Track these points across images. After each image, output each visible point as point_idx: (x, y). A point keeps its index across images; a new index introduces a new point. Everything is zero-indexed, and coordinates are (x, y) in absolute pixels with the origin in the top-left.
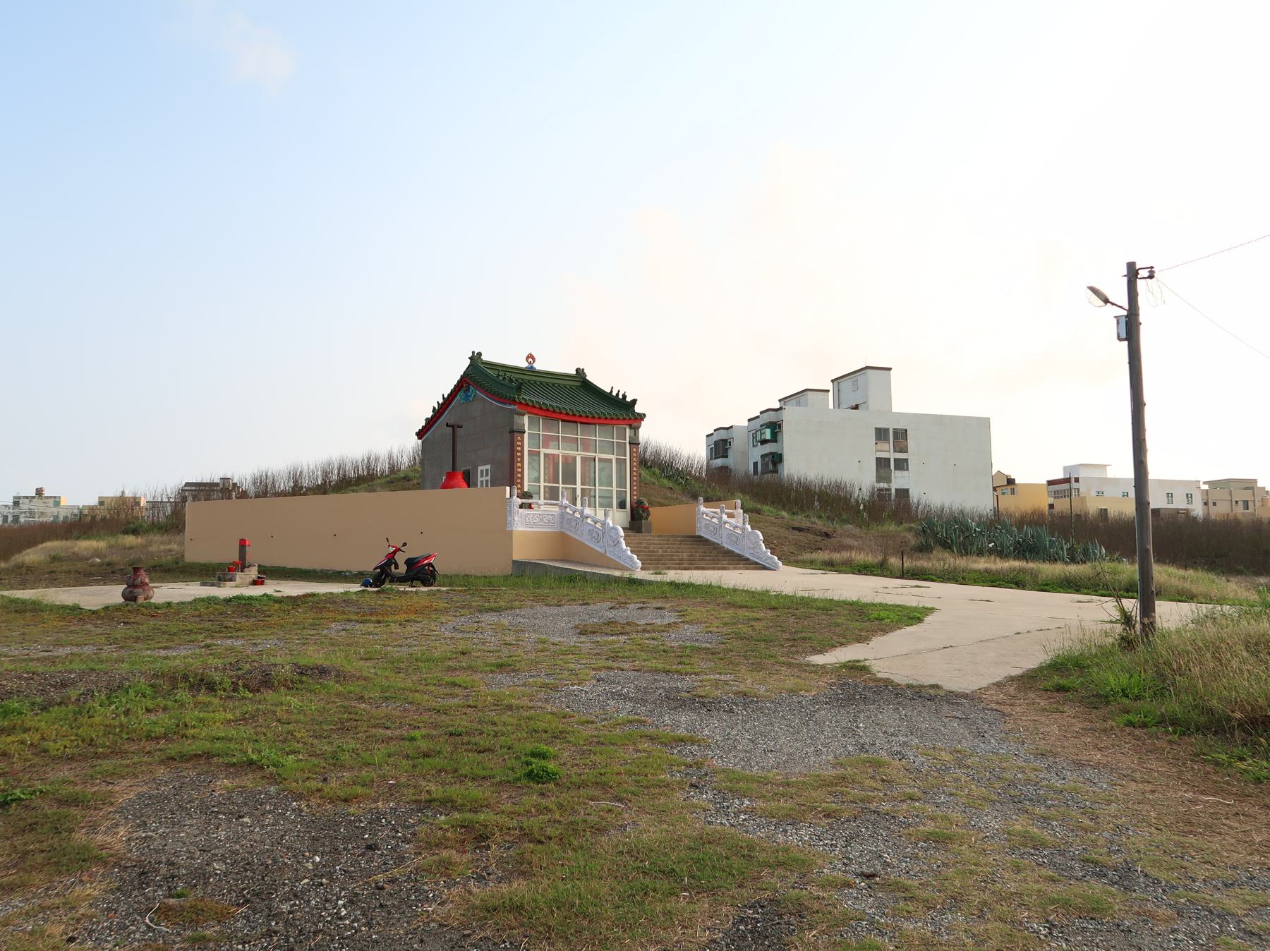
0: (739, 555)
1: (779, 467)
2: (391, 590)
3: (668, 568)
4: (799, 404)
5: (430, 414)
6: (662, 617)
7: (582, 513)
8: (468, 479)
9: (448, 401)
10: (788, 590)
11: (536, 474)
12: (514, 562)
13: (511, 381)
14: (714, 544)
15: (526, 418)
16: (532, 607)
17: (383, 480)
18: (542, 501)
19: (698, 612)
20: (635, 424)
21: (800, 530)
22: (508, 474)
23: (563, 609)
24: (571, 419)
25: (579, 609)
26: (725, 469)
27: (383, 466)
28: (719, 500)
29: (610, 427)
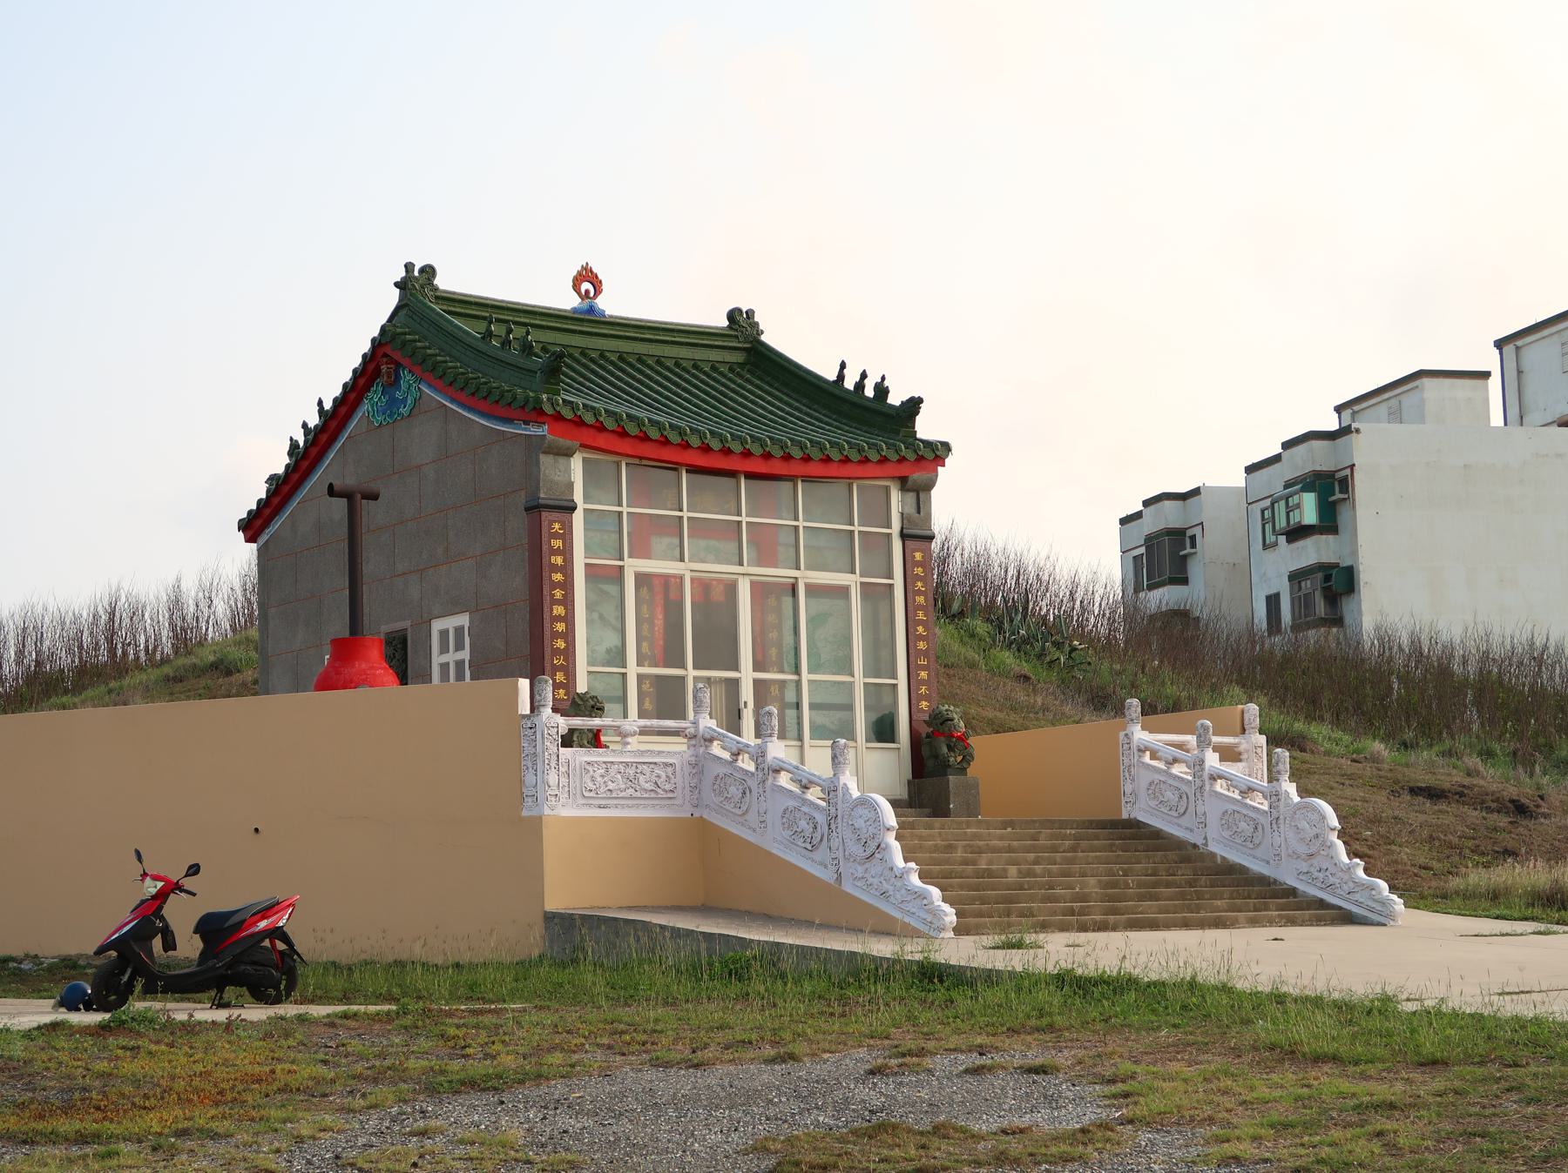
0: (1263, 881)
1: (1347, 607)
2: (146, 1019)
3: (1044, 927)
4: (1397, 416)
5: (279, 463)
6: (1052, 1101)
7: (759, 756)
8: (403, 659)
9: (335, 419)
10: (1467, 997)
11: (612, 640)
12: (550, 918)
13: (527, 348)
14: (1179, 845)
15: (576, 464)
16: (605, 1073)
17: (155, 674)
18: (633, 722)
19: (1175, 1082)
20: (917, 477)
21: (1434, 794)
22: (526, 640)
23: (712, 1078)
24: (715, 465)
25: (769, 1076)
26: (1181, 616)
27: (156, 630)
28: (1176, 707)
29: (839, 488)
